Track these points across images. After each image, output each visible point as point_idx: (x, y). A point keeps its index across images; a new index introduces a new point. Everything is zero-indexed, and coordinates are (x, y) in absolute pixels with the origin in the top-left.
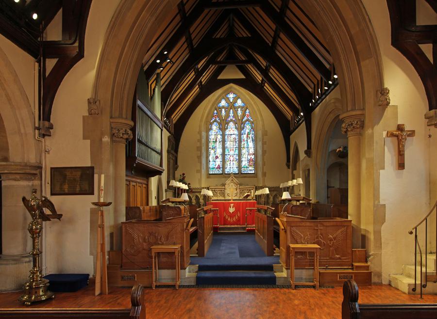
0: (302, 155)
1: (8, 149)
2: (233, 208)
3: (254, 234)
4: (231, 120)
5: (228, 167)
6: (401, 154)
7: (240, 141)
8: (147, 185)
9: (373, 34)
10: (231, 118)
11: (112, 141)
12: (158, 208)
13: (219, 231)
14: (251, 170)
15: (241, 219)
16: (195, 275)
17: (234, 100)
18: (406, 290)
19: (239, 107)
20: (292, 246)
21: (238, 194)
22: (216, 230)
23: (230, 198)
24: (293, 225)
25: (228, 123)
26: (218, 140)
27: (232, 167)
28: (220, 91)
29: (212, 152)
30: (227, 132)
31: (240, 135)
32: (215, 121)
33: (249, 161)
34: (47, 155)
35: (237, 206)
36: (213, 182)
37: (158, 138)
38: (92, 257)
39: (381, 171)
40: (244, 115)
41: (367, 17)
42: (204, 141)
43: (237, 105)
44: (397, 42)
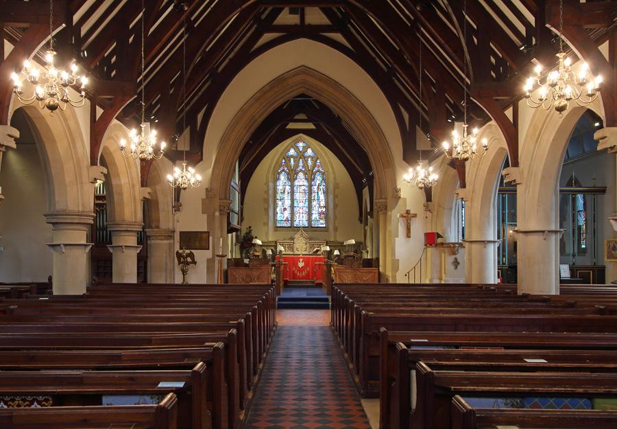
4: (301, 171)
5: (298, 219)
7: (310, 192)
10: (301, 168)
19: (309, 156)
22: (286, 282)
23: (299, 253)
25: (297, 174)
27: (301, 220)
28: (288, 141)
29: (280, 203)
30: (296, 183)
31: (310, 186)
32: (283, 170)
33: (320, 214)
35: (306, 261)
40: (314, 165)
42: (271, 192)
43: (306, 154)
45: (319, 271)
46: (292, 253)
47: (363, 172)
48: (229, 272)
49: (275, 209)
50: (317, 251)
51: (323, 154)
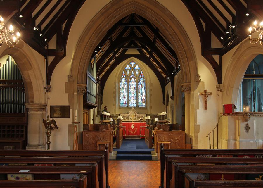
0: (170, 99)
1: (34, 98)
2: (133, 126)
3: (145, 140)
4: (133, 77)
5: (131, 103)
7: (137, 89)
8: (89, 113)
9: (193, 50)
10: (133, 75)
11: (78, 94)
12: (94, 125)
13: (126, 139)
14: (143, 105)
15: (138, 133)
16: (116, 155)
17: (134, 66)
19: (137, 70)
20: (158, 142)
21: (136, 119)
22: (124, 138)
23: (132, 121)
24: (159, 133)
25: (130, 79)
26: (125, 88)
27: (133, 103)
28: (126, 61)
29: (122, 94)
30: (130, 84)
31: (137, 85)
32: (124, 77)
33: (143, 100)
34: (48, 100)
35: (136, 125)
36: (122, 111)
37: (94, 88)
38: (69, 146)
39: (197, 110)
40: (139, 74)
41: (191, 43)
42: (117, 88)
43: (135, 68)
44: (204, 54)
45: (146, 133)
46: (128, 121)
47: (169, 72)
49: (119, 97)
50: (142, 119)
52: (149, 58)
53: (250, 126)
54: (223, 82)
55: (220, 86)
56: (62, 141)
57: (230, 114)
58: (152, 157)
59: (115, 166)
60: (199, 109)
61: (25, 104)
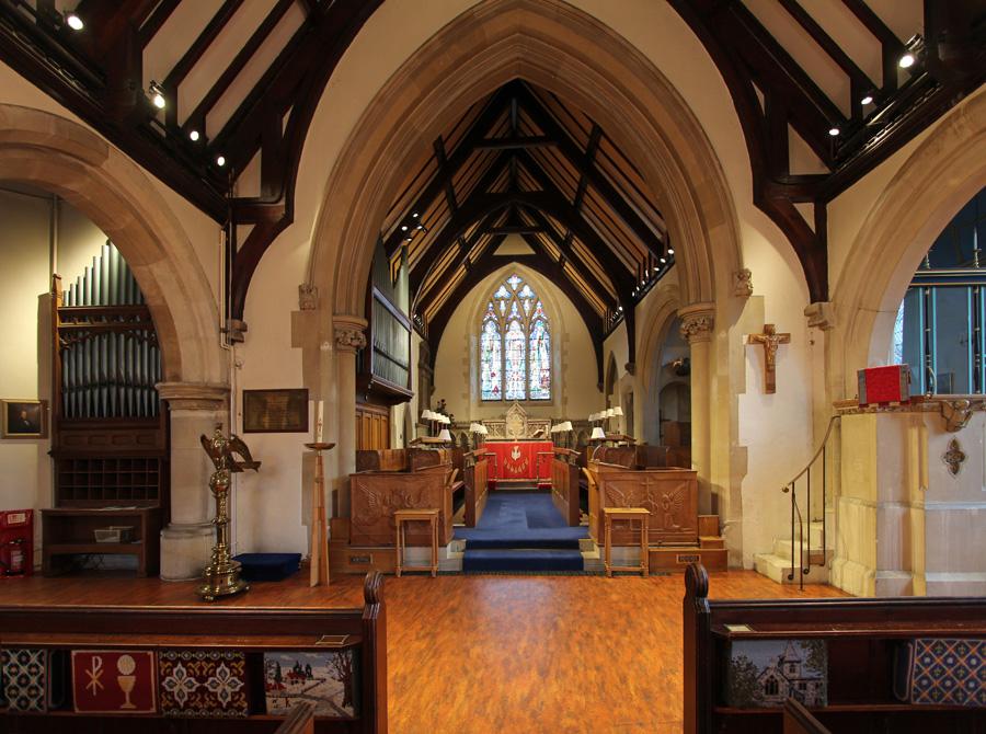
0: (622, 372)
4: (515, 318)
6: (769, 370)
7: (528, 350)
8: (388, 417)
9: (725, 185)
11: (336, 349)
17: (519, 287)
18: (778, 577)
19: (526, 298)
22: (492, 487)
23: (513, 437)
25: (509, 323)
27: (516, 390)
28: (496, 274)
29: (485, 366)
30: (509, 336)
31: (528, 340)
32: (490, 319)
34: (238, 371)
35: (524, 449)
36: (487, 413)
37: (405, 344)
40: (533, 311)
41: (716, 162)
43: (522, 295)
44: (761, 200)
48: (353, 483)
50: (540, 433)
51: (546, 291)
52: (561, 264)
53: (964, 448)
54: (831, 294)
55: (820, 308)
56: (280, 508)
57: (891, 404)
58: (585, 562)
59: (453, 610)
60: (744, 392)
61: (157, 386)
